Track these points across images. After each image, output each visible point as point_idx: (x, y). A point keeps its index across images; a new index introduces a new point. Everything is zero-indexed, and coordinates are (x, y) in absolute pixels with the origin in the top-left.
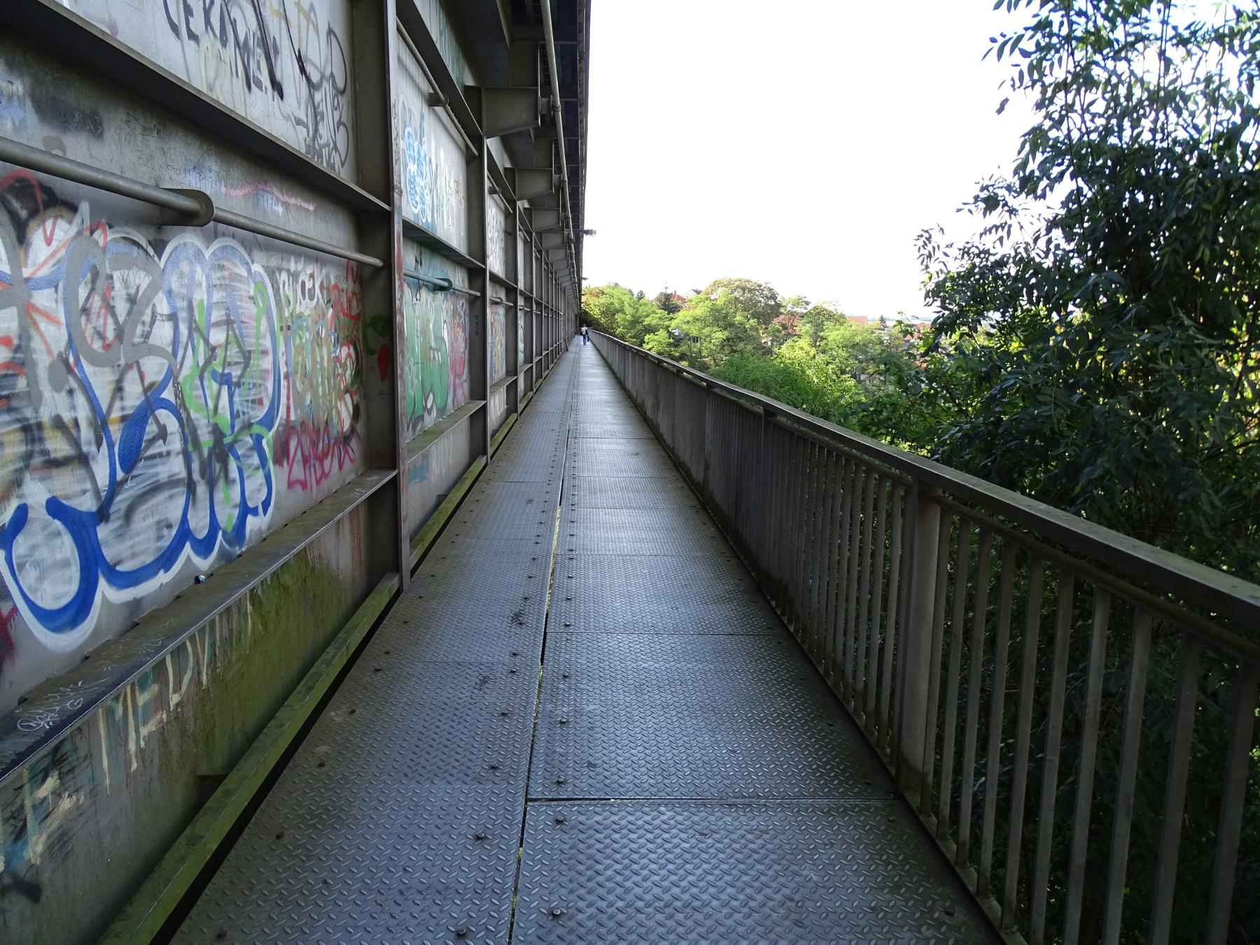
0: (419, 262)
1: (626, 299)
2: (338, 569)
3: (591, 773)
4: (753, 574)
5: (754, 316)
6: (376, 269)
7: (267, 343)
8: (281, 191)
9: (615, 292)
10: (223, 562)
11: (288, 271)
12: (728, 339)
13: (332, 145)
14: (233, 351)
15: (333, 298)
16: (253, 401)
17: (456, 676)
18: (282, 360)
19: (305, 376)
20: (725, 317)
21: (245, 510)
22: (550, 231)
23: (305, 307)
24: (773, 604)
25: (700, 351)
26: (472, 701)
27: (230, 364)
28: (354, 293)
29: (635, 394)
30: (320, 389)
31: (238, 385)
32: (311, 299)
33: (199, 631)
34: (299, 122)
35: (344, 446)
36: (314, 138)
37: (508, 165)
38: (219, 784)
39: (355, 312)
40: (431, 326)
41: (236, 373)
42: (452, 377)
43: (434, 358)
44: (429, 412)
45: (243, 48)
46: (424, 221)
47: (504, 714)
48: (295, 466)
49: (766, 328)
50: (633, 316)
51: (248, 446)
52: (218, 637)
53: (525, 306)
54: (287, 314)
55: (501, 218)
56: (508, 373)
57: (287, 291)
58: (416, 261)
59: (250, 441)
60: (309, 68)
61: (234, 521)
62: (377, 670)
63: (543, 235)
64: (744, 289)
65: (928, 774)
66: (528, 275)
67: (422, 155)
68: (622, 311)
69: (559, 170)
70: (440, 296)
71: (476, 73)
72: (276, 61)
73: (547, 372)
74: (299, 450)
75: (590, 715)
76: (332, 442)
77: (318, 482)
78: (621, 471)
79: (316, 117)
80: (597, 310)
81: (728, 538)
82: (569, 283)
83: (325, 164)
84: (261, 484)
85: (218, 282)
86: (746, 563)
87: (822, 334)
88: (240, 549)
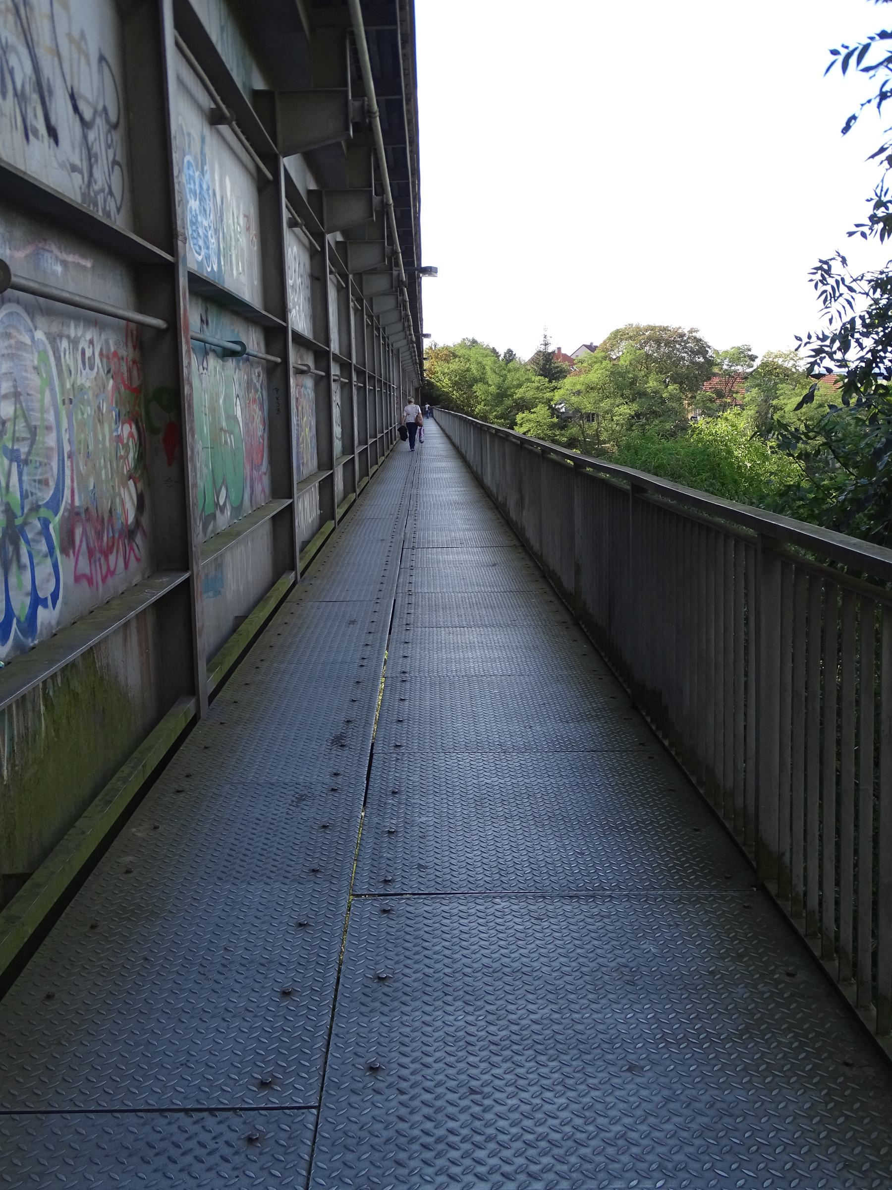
0: (204, 321)
1: (488, 362)
2: (127, 685)
3: (421, 874)
4: (629, 691)
5: (674, 380)
6: (159, 331)
7: (51, 417)
8: (60, 248)
9: (472, 353)
10: (18, 652)
11: (68, 337)
12: (638, 415)
13: (107, 190)
14: (21, 425)
15: (113, 368)
16: (40, 481)
17: (269, 795)
18: (66, 437)
19: (88, 457)
20: (633, 383)
21: (37, 601)
22: (372, 271)
23: (86, 378)
24: (649, 719)
25: (597, 435)
26: (288, 817)
27: (18, 440)
28: (134, 362)
29: (495, 491)
30: (103, 472)
31: (26, 462)
32: (92, 369)
33: (17, 702)
34: (74, 168)
35: (129, 541)
36: (89, 185)
37: (313, 186)
38: (25, 882)
39: (136, 383)
40: (221, 401)
41: (24, 449)
42: (248, 467)
43: (226, 441)
44: (222, 509)
45: (21, 97)
46: (209, 269)
47: (325, 827)
48: (80, 558)
49: (693, 397)
50: (499, 387)
51: (36, 531)
52: (16, 732)
53: (342, 376)
54: (68, 386)
55: (305, 258)
56: (320, 467)
57: (68, 359)
58: (202, 320)
59: (38, 525)
60: (82, 106)
61: (27, 610)
62: (178, 792)
63: (365, 278)
64: (658, 342)
65: (783, 854)
66: (344, 335)
67: (205, 187)
68: (482, 380)
69: (381, 191)
70: (231, 363)
71: (267, 72)
72: (51, 103)
73: (375, 467)
74: (84, 540)
75: (422, 825)
76: (117, 535)
77: (104, 580)
78: (472, 585)
79: (90, 159)
80: (446, 381)
81: (603, 654)
82: (404, 342)
83: (100, 213)
84: (50, 574)
85: (6, 352)
86: (621, 679)
87: (774, 402)
88: (33, 641)
